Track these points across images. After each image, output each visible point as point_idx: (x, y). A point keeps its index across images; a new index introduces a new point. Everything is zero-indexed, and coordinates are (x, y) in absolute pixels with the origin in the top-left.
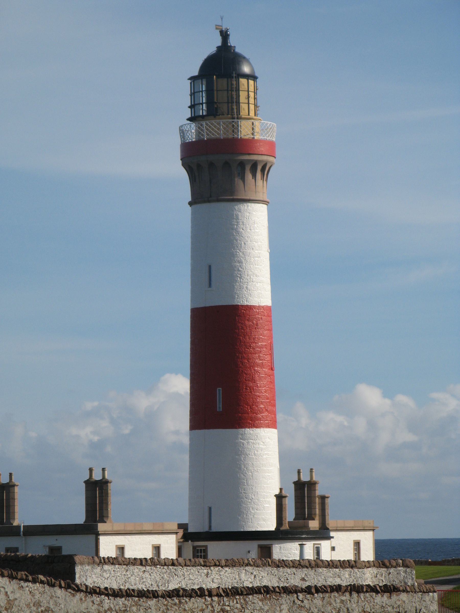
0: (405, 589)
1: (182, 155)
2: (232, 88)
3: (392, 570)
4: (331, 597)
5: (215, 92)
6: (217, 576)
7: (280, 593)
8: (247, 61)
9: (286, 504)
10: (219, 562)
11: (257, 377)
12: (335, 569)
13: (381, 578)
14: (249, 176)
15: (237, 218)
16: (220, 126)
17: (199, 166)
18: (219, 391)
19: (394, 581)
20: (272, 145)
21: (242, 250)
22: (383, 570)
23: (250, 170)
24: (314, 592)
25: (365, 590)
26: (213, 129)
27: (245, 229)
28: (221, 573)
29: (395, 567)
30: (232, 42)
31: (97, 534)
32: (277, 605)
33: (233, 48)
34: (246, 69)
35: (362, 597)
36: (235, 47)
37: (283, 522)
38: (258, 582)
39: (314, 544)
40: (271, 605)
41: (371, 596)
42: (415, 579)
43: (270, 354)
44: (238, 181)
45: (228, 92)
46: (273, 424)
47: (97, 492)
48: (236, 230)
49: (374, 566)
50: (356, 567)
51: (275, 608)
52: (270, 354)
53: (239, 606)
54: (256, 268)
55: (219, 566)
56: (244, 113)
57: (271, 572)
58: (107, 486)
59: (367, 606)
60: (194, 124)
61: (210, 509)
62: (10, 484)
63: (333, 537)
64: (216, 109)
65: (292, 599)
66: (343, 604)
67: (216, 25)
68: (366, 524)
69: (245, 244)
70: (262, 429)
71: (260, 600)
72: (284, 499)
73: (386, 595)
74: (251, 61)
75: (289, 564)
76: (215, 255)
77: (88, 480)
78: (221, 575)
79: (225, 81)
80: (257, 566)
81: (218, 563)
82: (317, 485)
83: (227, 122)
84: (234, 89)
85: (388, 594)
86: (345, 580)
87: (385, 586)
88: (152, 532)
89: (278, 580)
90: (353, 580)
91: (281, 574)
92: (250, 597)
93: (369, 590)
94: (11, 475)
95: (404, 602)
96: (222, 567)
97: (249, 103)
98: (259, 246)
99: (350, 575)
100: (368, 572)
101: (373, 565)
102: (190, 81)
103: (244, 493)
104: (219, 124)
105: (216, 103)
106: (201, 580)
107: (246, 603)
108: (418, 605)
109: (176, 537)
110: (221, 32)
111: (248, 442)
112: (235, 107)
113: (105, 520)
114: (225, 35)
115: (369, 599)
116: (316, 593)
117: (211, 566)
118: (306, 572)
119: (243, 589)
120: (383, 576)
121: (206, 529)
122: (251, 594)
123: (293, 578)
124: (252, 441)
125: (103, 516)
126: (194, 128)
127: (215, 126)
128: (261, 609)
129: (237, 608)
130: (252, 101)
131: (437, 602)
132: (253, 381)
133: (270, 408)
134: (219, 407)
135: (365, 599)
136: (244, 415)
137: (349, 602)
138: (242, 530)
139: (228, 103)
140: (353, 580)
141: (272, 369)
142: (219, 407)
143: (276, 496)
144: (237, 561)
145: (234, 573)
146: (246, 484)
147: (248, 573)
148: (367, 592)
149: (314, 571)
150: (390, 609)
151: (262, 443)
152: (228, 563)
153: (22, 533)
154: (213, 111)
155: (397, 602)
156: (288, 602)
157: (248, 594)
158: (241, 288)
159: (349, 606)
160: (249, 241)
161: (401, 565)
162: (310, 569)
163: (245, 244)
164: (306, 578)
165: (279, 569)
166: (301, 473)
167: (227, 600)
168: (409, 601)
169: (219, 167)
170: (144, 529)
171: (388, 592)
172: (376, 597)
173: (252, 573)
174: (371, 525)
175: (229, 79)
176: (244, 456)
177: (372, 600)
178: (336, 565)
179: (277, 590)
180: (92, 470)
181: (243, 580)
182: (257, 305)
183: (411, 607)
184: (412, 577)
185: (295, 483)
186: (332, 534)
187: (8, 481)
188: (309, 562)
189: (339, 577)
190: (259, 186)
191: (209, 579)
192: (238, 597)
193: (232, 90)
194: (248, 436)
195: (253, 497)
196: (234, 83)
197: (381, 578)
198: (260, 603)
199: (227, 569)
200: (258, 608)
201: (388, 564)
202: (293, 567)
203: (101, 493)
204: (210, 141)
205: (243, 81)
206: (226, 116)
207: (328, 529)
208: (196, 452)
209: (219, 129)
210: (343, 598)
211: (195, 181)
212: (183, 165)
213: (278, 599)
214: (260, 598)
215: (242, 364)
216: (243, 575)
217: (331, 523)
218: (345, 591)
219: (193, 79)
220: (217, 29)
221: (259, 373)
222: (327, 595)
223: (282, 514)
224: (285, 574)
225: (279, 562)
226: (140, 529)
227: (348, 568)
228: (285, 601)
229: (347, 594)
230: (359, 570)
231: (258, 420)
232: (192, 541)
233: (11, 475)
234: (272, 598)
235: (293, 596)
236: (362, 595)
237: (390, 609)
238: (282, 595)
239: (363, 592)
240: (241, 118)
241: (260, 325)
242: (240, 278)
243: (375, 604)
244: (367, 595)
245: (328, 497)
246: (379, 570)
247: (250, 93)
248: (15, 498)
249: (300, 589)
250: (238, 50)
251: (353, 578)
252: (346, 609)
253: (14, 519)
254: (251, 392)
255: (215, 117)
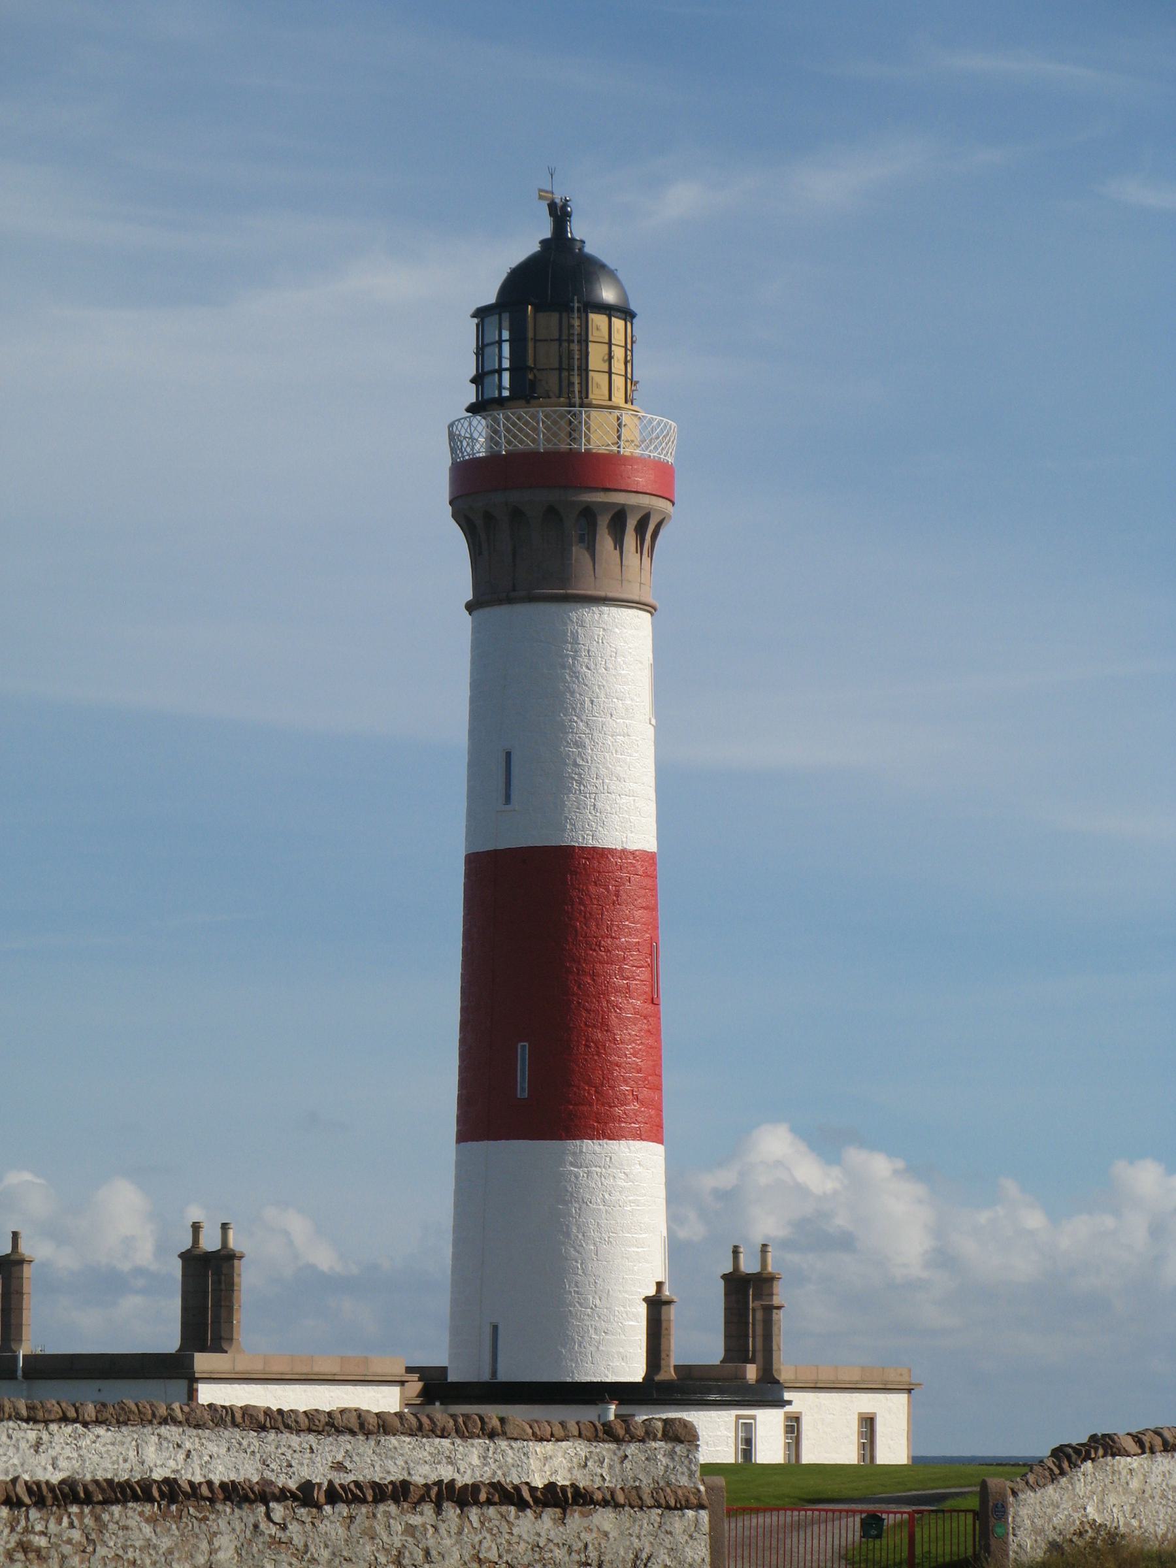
0: (609, 1497)
1: (451, 493)
2: (570, 334)
3: (632, 1449)
4: (374, 1516)
5: (530, 345)
6: (68, 1451)
7: (212, 1501)
8: (612, 275)
9: (669, 1321)
10: (77, 1411)
11: (613, 1020)
12: (438, 1440)
13: (599, 1471)
14: (605, 543)
15: (576, 641)
16: (538, 423)
17: (488, 517)
18: (523, 1049)
19: (635, 1479)
20: (664, 472)
21: (584, 718)
22: (606, 1449)
23: (609, 526)
24: (322, 1499)
25: (483, 1497)
26: (521, 430)
27: (592, 666)
28: (83, 1443)
29: (642, 1441)
30: (577, 229)
31: (192, 1380)
32: (202, 1536)
33: (578, 245)
34: (608, 295)
35: (474, 1519)
36: (583, 242)
37: (663, 1363)
38: (198, 1471)
39: (738, 1417)
40: (183, 1535)
41: (502, 1516)
42: (698, 1474)
43: (651, 966)
44: (578, 553)
45: (560, 345)
46: (654, 1133)
47: (208, 1280)
48: (571, 668)
49: (580, 1436)
50: (504, 1434)
51: (194, 1545)
52: (651, 966)
53: (76, 1535)
54: (618, 760)
55: (75, 1421)
56: (597, 394)
57: (240, 1444)
58: (232, 1266)
59: (485, 1544)
60: (483, 422)
61: (495, 1328)
62: (12, 1257)
63: (789, 1403)
64: (533, 384)
65: (251, 1520)
66: (413, 1536)
67: (541, 190)
68: (892, 1376)
69: (592, 702)
70: (623, 1142)
71: (147, 1521)
72: (664, 1308)
73: (549, 1514)
74: (620, 275)
75: (297, 1422)
76: (523, 726)
77: (188, 1251)
78: (80, 1448)
79: (554, 317)
80: (197, 1426)
81: (72, 1414)
82: (775, 1283)
83: (555, 412)
84: (576, 338)
85: (558, 1510)
86: (469, 1472)
87: (551, 1487)
88: (337, 1378)
89: (259, 1466)
90: (495, 1473)
91: (271, 1448)
92: (116, 1509)
93: (496, 1498)
94: (15, 1235)
95: (606, 1534)
96: (85, 1425)
97: (610, 373)
98: (627, 710)
99: (485, 1458)
100: (560, 1454)
101: (576, 1433)
102: (475, 320)
103: (577, 1293)
104: (534, 417)
105: (531, 369)
106: (16, 1461)
107: (102, 1526)
108: (647, 1544)
109: (402, 1393)
110: (552, 206)
111: (589, 1173)
112: (576, 380)
113: (225, 1347)
114: (560, 214)
115: (497, 1523)
116: (326, 1504)
117: (52, 1421)
118: (349, 1447)
119: (91, 1488)
120: (605, 1465)
121: (486, 1377)
122: (116, 1502)
123: (306, 1462)
124: (598, 1169)
125: (221, 1338)
126: (484, 434)
127: (527, 423)
128: (149, 1545)
129: (69, 1541)
130: (618, 366)
131: (707, 1537)
132: (605, 1027)
133: (645, 1093)
134: (522, 1090)
135: (482, 1523)
136: (581, 1108)
137: (431, 1530)
138: (569, 1380)
139: (560, 369)
140: (495, 1473)
141: (654, 1001)
142: (522, 1090)
143: (647, 1300)
144: (134, 1408)
145: (123, 1443)
146: (580, 1272)
147: (165, 1444)
148: (489, 1502)
149: (373, 1443)
150: (559, 1554)
151: (622, 1176)
152: (106, 1415)
153: (20, 1373)
154: (526, 390)
155: (583, 1535)
156: (238, 1526)
157: (106, 1502)
158: (580, 807)
159: (431, 1543)
160: (602, 695)
161: (659, 1435)
162: (361, 1437)
163: (592, 702)
164: (347, 1464)
165: (263, 1434)
166: (741, 1255)
167: (38, 1515)
168: (622, 1534)
169: (537, 519)
170: (316, 1369)
171: (555, 1506)
172: (517, 1517)
173: (179, 1446)
174: (906, 1378)
175: (564, 315)
176: (576, 1205)
177: (505, 1528)
178: (443, 1430)
179: (205, 1491)
180: (200, 1227)
181: (150, 1462)
182: (619, 848)
183: (626, 1550)
184: (689, 1469)
185: (725, 1277)
186: (787, 1396)
187: (9, 1251)
188: (359, 1416)
189: (451, 1463)
190: (634, 569)
191: (44, 1459)
192: (74, 1509)
193: (570, 341)
194: (589, 1157)
195: (598, 1302)
196: (576, 323)
197: (599, 1471)
198: (147, 1529)
199: (101, 1430)
200: (137, 1544)
201: (621, 1432)
202: (310, 1430)
203: (217, 1283)
204: (513, 458)
205: (598, 321)
206: (554, 400)
207: (778, 1382)
208: (472, 1197)
209: (535, 430)
210: (416, 1520)
211: (480, 553)
212: (455, 516)
213: (206, 1519)
214: (147, 1514)
215: (579, 987)
216: (152, 1449)
217: (785, 1371)
218: (421, 1500)
219: (481, 314)
220: (541, 197)
221: (620, 1009)
222: (364, 1510)
223: (659, 1344)
224: (283, 1449)
225: (266, 1413)
226: (305, 1369)
227: (479, 1437)
228: (229, 1525)
229: (428, 1509)
230: (513, 1444)
231: (614, 1121)
232: (442, 1404)
233: (15, 1235)
234: (184, 1513)
235: (253, 1511)
236: (474, 1513)
237: (559, 1554)
238: (219, 1507)
239: (476, 1502)
240: (590, 405)
241: (624, 897)
242: (580, 783)
243: (514, 1540)
244: (491, 1511)
245: (779, 1308)
246: (593, 1449)
247: (613, 347)
248: (25, 1290)
249: (277, 1491)
250: (589, 249)
251: (493, 1466)
252: (421, 1553)
253: (20, 1340)
254: (598, 1054)
255: (528, 402)
